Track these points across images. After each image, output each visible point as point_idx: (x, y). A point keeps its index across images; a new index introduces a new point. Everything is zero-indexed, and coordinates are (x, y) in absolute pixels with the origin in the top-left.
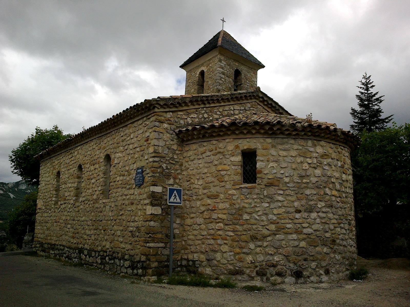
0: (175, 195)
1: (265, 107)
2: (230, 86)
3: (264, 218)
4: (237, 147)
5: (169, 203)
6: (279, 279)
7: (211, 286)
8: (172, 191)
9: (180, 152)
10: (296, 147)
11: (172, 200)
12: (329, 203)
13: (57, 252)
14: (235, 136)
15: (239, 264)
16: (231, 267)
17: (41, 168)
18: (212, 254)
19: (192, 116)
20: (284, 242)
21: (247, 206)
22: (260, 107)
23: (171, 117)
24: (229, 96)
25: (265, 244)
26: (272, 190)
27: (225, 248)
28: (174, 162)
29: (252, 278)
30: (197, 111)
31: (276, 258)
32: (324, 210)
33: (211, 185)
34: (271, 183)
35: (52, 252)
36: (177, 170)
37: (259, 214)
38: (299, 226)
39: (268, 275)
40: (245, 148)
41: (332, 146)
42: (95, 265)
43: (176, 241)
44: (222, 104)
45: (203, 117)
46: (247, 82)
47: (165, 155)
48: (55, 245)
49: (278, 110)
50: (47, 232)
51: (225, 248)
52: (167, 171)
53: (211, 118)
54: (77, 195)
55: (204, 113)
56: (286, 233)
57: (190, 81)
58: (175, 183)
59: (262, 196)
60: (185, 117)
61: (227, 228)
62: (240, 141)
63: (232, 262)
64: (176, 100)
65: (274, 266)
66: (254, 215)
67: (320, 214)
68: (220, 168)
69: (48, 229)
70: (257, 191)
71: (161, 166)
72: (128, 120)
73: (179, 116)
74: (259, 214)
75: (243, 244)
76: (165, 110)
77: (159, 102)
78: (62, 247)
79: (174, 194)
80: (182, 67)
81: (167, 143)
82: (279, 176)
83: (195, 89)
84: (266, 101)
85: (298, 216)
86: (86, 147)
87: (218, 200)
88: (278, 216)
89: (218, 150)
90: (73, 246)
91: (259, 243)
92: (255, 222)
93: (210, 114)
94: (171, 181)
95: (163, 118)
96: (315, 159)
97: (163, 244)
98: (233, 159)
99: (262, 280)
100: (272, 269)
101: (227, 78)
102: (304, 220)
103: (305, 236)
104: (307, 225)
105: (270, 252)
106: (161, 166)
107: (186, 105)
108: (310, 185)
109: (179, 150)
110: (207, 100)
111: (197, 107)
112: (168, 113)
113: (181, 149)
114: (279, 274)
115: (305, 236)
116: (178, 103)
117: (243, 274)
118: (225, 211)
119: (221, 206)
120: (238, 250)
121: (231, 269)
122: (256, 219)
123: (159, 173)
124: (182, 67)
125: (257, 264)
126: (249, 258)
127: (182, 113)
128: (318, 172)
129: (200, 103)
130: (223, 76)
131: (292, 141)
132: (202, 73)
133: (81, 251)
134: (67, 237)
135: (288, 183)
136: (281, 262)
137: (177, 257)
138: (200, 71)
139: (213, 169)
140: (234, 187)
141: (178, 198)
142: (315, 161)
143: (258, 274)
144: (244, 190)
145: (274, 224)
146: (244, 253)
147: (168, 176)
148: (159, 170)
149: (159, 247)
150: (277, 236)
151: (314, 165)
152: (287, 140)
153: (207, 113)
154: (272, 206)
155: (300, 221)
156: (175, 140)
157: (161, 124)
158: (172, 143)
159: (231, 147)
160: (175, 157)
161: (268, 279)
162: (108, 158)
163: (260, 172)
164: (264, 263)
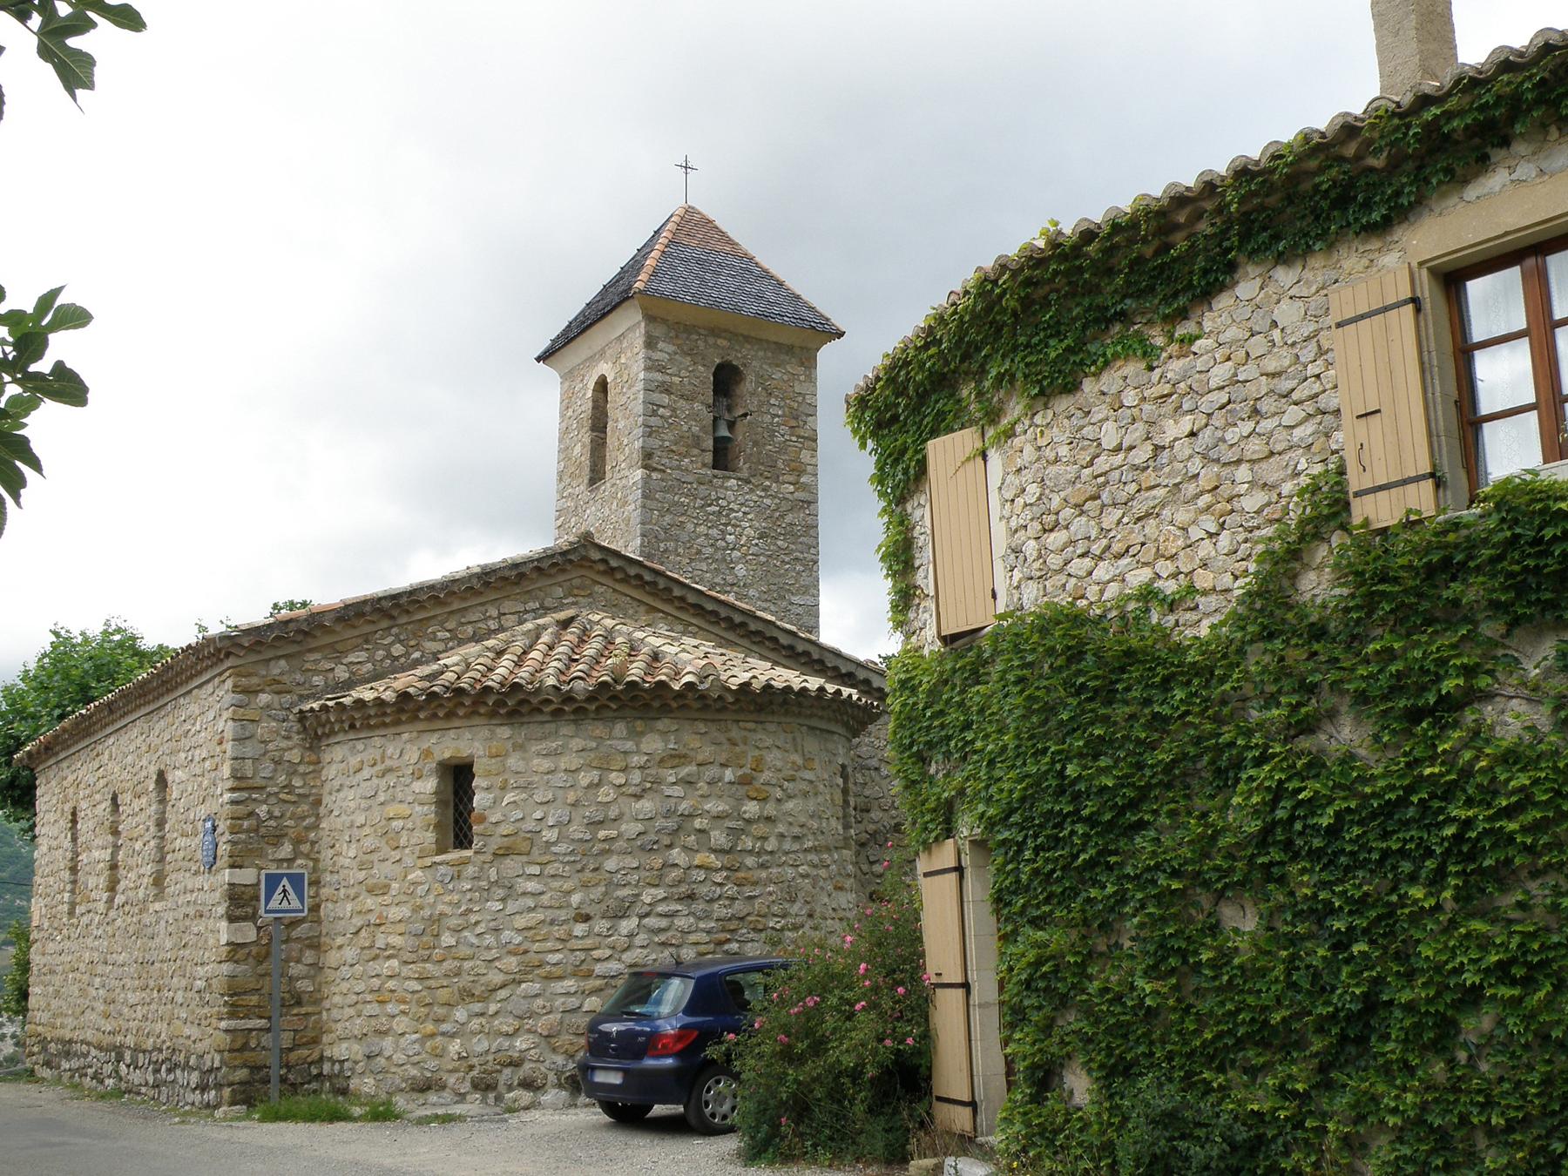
0: (284, 891)
1: (617, 587)
2: (695, 429)
3: (489, 939)
4: (427, 753)
5: (267, 912)
6: (526, 1097)
7: (355, 1120)
8: (273, 881)
9: (311, 768)
10: (577, 743)
11: (273, 904)
12: (683, 889)
13: (75, 1063)
14: (421, 726)
15: (432, 1064)
16: (414, 1072)
17: (38, 792)
18: (377, 1040)
19: (351, 658)
20: (540, 1002)
21: (448, 910)
22: (602, 589)
23: (282, 674)
24: (475, 581)
25: (493, 1008)
26: (511, 865)
27: (401, 1024)
28: (293, 798)
29: (462, 1097)
30: (367, 642)
31: (520, 1043)
32: (660, 909)
33: (375, 857)
34: (508, 848)
35: (65, 1065)
36: (303, 818)
37: (479, 930)
38: (582, 955)
39: (501, 1088)
40: (447, 755)
41: (702, 727)
42: (143, 1090)
43: (303, 1010)
44: (455, 606)
45: (389, 655)
46: (772, 401)
47: (263, 783)
48: (70, 1041)
49: (668, 590)
50: (55, 1003)
51: (401, 1024)
52: (272, 823)
53: (417, 655)
54: (112, 887)
55: (392, 644)
56: (549, 978)
57: (570, 413)
58: (297, 854)
59: (484, 884)
60: (328, 666)
61: (405, 971)
62: (434, 738)
63: (417, 1058)
64: (292, 626)
65: (515, 1064)
66: (466, 933)
67: (651, 922)
68: (391, 810)
69: (57, 994)
70: (470, 870)
71: (251, 814)
72: (192, 677)
73: (308, 666)
74: (479, 930)
75: (440, 1011)
76: (260, 657)
77: (238, 641)
78: (84, 1048)
79: (280, 889)
80: (544, 357)
81: (271, 746)
82: (530, 825)
83: (584, 446)
84: (619, 568)
85: (580, 929)
86: (124, 738)
87: (387, 899)
88: (526, 934)
89: (388, 763)
90: (107, 1040)
91: (477, 1007)
92: (469, 952)
93: (412, 643)
94: (286, 850)
95: (255, 680)
96: (638, 772)
97: (264, 1021)
98: (418, 786)
99: (484, 1101)
100: (508, 1071)
101: (682, 403)
102: (598, 939)
103: (598, 982)
104: (608, 952)
105: (505, 1028)
106: (251, 814)
107: (328, 631)
108: (621, 844)
109: (310, 763)
110: (397, 605)
111: (368, 629)
112: (272, 663)
113: (314, 757)
114: (527, 1084)
115: (598, 982)
116: (299, 631)
117: (444, 1087)
118: (401, 928)
119: (395, 913)
120: (430, 1027)
121: (414, 1078)
122: (472, 945)
123: (248, 831)
124: (544, 357)
125: (475, 1061)
126: (455, 1047)
127: (317, 656)
128: (646, 806)
129: (374, 618)
130: (666, 399)
131: (566, 730)
132: (602, 385)
133: (119, 1051)
134: (93, 1017)
135: (555, 844)
136: (532, 1052)
137: (306, 1052)
138: (595, 378)
139: (376, 815)
140: (420, 863)
141: (292, 895)
142: (636, 777)
143: (475, 1086)
144: (442, 869)
145: (516, 954)
146: (443, 1034)
147: (277, 838)
148: (246, 824)
149: (250, 1030)
150: (523, 985)
151: (632, 790)
152: (553, 725)
153: (400, 642)
154: (511, 907)
155: (588, 943)
156: (296, 737)
157: (252, 697)
158: (284, 744)
159: (412, 755)
160: (297, 782)
161: (499, 1099)
162: (161, 781)
163: (482, 819)
164: (490, 1058)
